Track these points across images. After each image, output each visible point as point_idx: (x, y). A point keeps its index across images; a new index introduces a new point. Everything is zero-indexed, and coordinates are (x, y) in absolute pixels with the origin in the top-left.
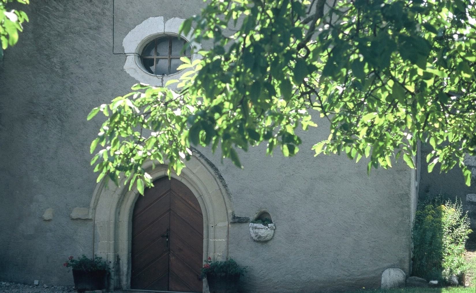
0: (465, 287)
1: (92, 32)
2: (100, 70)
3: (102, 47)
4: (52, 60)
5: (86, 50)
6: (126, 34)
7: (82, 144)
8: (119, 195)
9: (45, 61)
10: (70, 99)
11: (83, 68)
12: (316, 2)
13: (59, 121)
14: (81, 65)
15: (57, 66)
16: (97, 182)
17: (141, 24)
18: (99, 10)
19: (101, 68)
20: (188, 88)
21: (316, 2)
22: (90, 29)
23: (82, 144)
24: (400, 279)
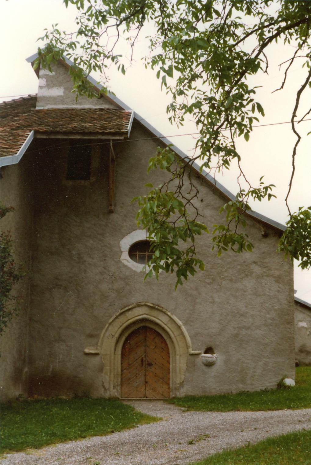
0: (252, 251)
1: (99, 237)
2: (105, 260)
3: (106, 246)
4: (72, 252)
5: (95, 247)
6: (122, 238)
7: (92, 306)
8: (116, 338)
9: (67, 253)
10: (84, 277)
11: (93, 258)
12: (290, 420)
13: (76, 291)
14: (92, 256)
15: (75, 256)
16: (298, 9)
17: (131, 233)
18: (104, 223)
19: (105, 259)
20: (114, 380)
21: (290, 420)
22: (98, 234)
23: (92, 306)
24: (238, 247)
